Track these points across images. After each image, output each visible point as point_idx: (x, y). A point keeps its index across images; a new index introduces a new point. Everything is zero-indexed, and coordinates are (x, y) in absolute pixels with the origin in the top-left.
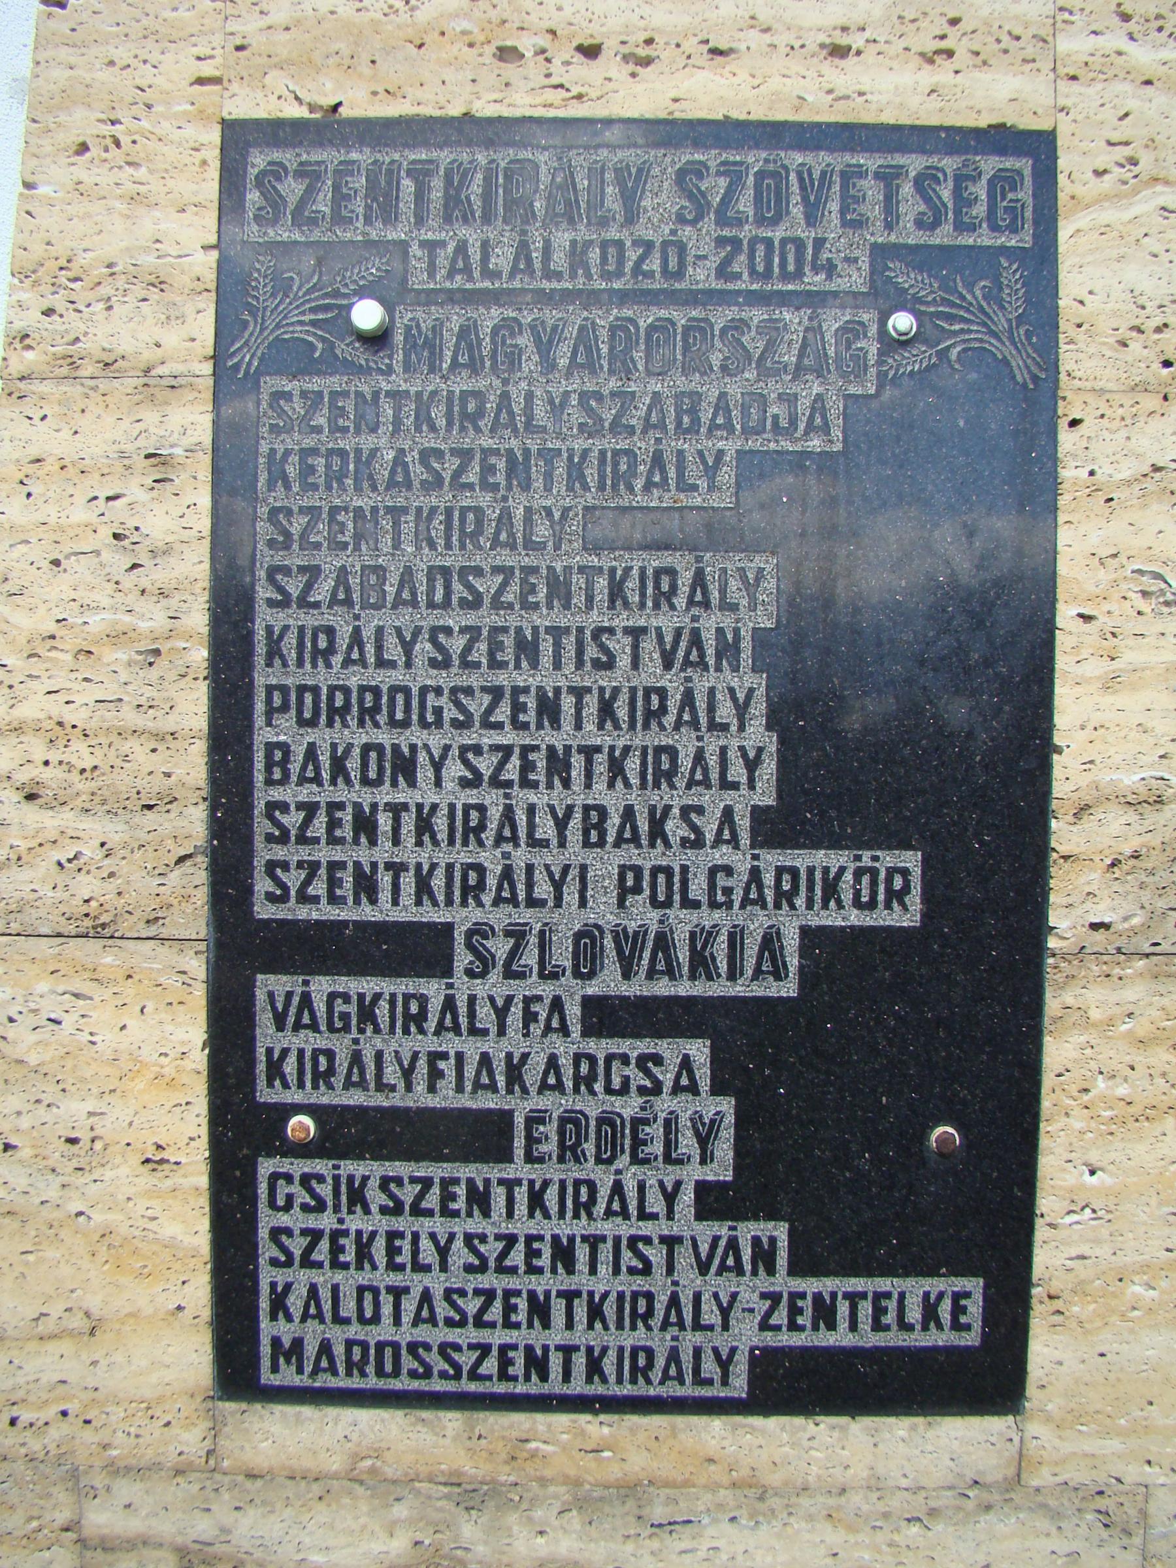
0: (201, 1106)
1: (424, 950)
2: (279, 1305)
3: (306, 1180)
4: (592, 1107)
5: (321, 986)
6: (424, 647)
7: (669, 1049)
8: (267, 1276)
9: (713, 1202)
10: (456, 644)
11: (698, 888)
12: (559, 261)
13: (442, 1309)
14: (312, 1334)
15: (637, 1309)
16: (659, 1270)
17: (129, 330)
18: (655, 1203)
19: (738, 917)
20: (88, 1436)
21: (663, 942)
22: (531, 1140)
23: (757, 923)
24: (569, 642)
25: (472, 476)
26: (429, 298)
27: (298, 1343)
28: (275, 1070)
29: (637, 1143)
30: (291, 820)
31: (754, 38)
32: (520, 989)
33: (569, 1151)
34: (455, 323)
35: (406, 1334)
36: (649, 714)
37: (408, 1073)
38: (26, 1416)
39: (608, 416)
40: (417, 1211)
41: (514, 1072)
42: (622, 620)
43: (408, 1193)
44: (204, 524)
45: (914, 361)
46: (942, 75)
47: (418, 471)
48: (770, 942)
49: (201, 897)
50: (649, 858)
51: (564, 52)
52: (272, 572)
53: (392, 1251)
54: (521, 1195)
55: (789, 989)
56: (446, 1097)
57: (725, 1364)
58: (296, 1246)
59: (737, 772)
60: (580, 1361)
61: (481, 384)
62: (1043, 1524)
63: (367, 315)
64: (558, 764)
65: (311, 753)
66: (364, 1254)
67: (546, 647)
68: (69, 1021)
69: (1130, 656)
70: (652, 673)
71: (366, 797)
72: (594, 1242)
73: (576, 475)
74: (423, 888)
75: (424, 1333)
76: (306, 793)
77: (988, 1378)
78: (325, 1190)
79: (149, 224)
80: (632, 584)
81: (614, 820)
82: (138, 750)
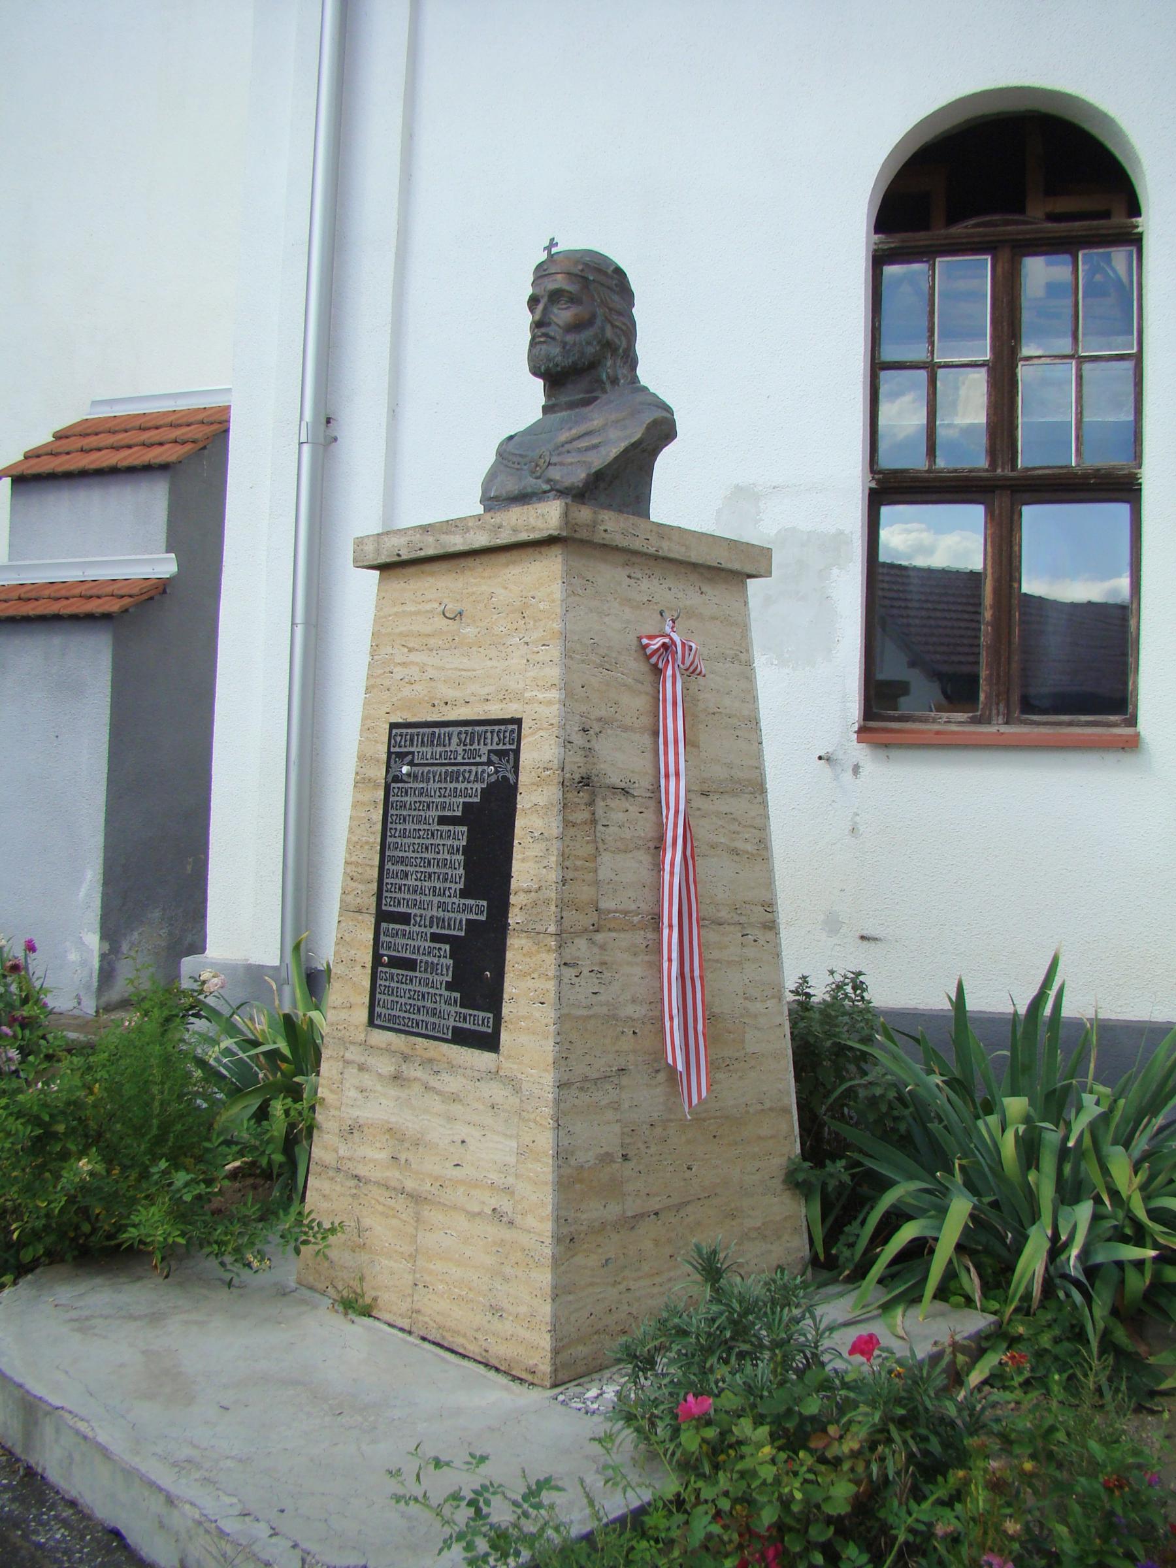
55: (463, 934)
82: (368, 868)
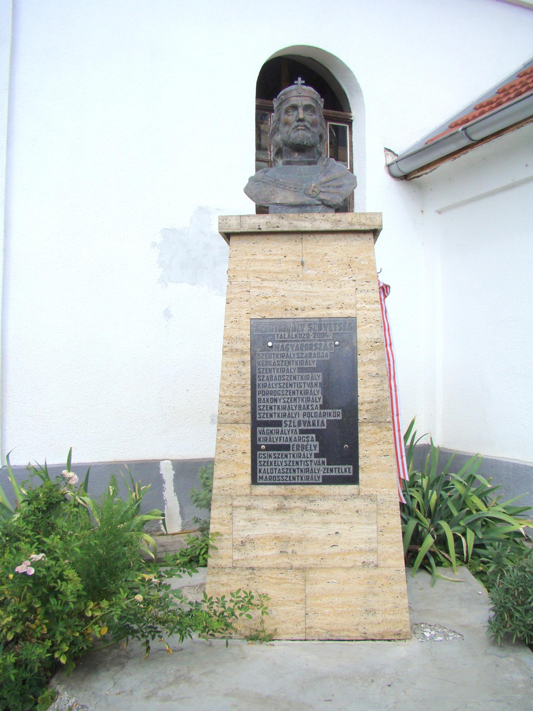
0: (250, 445)
1: (278, 424)
2: (260, 471)
3: (264, 454)
4: (300, 443)
5: (266, 429)
6: (278, 385)
7: (310, 436)
8: (258, 467)
9: (316, 456)
10: (282, 385)
11: (313, 415)
12: (294, 336)
13: (281, 471)
14: (264, 475)
15: (307, 470)
16: (310, 465)
17: (239, 346)
18: (309, 456)
19: (318, 418)
20: (234, 491)
21: (309, 422)
22: (293, 448)
23: (321, 419)
24: (296, 384)
25: (283, 364)
26: (278, 341)
27: (262, 477)
28: (260, 440)
29: (306, 448)
30: (262, 407)
31: (317, 307)
32: (291, 428)
33: (298, 449)
34: (281, 344)
35: (277, 475)
36: (306, 393)
37: (277, 440)
38: (225, 489)
39: (300, 356)
40: (278, 458)
41: (290, 439)
42: (303, 381)
43: (277, 456)
44: (250, 370)
45: (338, 348)
46: (341, 311)
47: (277, 363)
48: (323, 421)
49: (250, 418)
50: (307, 411)
51: (294, 309)
52: (259, 376)
53: (275, 463)
54: (292, 455)
55: (325, 427)
56: (282, 443)
57: (319, 478)
58: (262, 463)
59: (318, 400)
60: (300, 478)
61: (284, 352)
62: (363, 500)
63: (270, 344)
64: (295, 399)
65: (264, 399)
66: (271, 464)
67: (293, 385)
68: (232, 435)
69: (368, 384)
70: (307, 388)
71: (271, 404)
72: (301, 461)
73: (296, 363)
74: (278, 416)
75: (279, 474)
76: (263, 404)
77: (353, 479)
78: (266, 455)
79: (241, 332)
80: (304, 377)
81: (302, 406)
82: (242, 399)
